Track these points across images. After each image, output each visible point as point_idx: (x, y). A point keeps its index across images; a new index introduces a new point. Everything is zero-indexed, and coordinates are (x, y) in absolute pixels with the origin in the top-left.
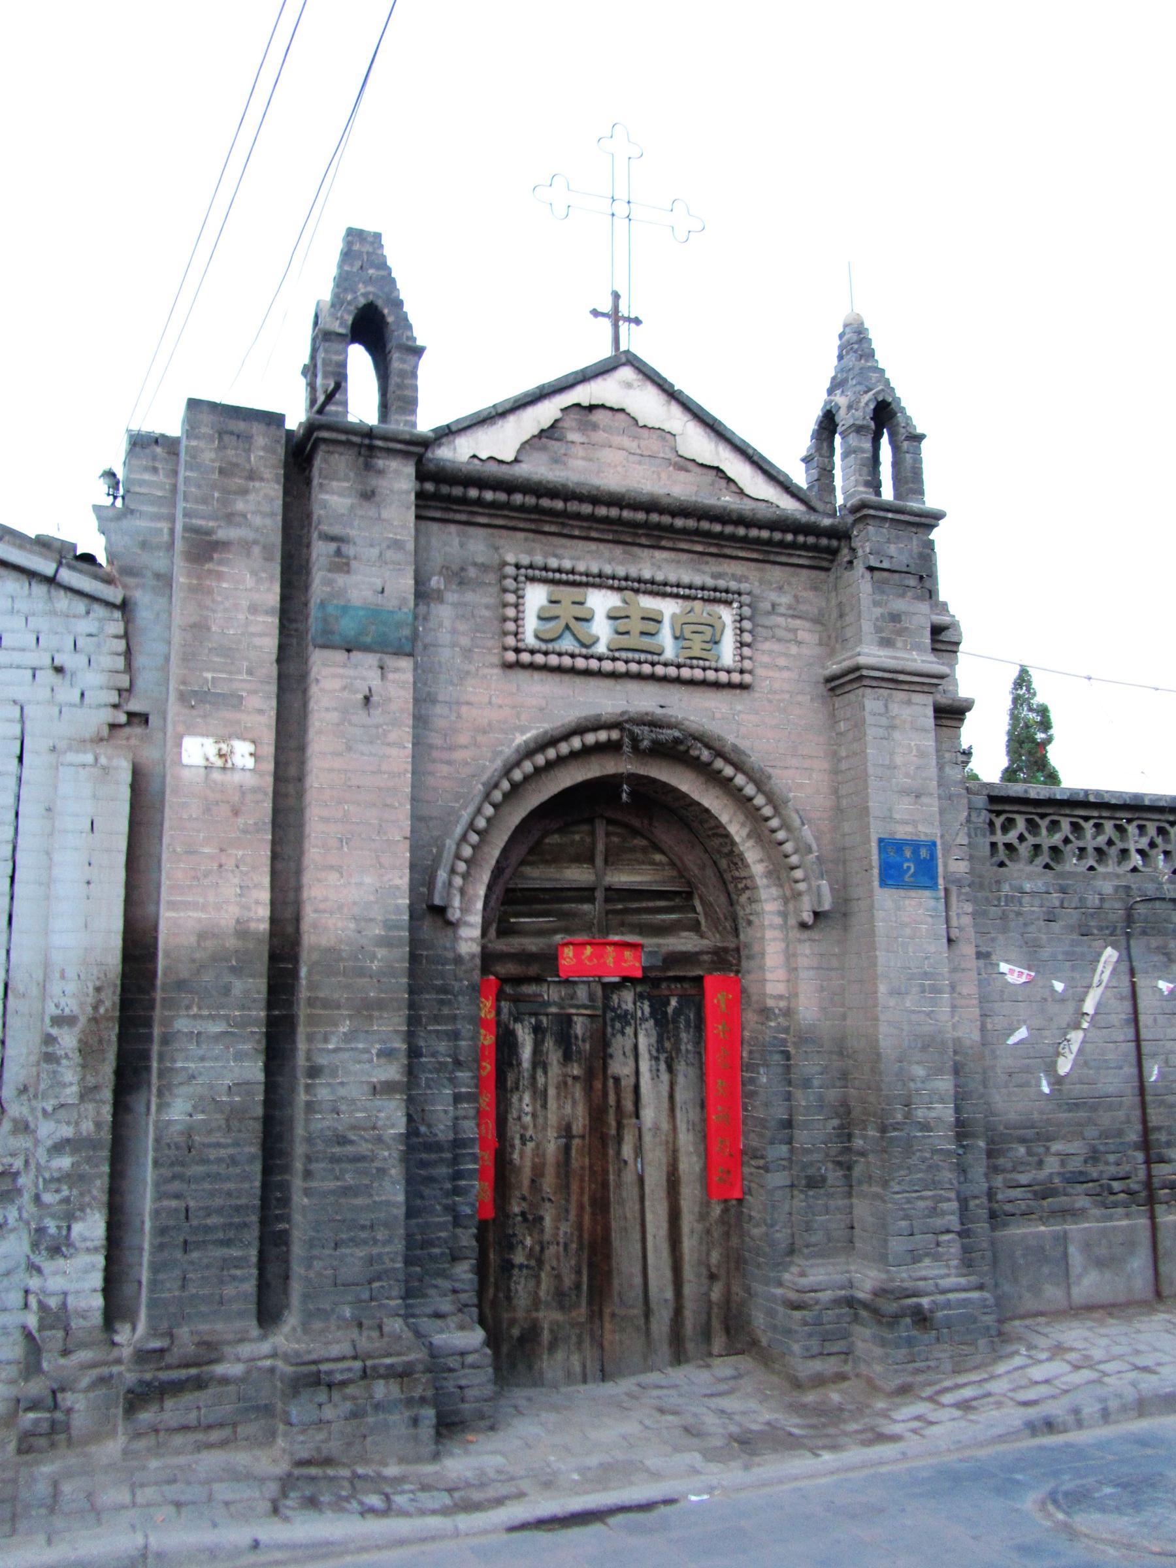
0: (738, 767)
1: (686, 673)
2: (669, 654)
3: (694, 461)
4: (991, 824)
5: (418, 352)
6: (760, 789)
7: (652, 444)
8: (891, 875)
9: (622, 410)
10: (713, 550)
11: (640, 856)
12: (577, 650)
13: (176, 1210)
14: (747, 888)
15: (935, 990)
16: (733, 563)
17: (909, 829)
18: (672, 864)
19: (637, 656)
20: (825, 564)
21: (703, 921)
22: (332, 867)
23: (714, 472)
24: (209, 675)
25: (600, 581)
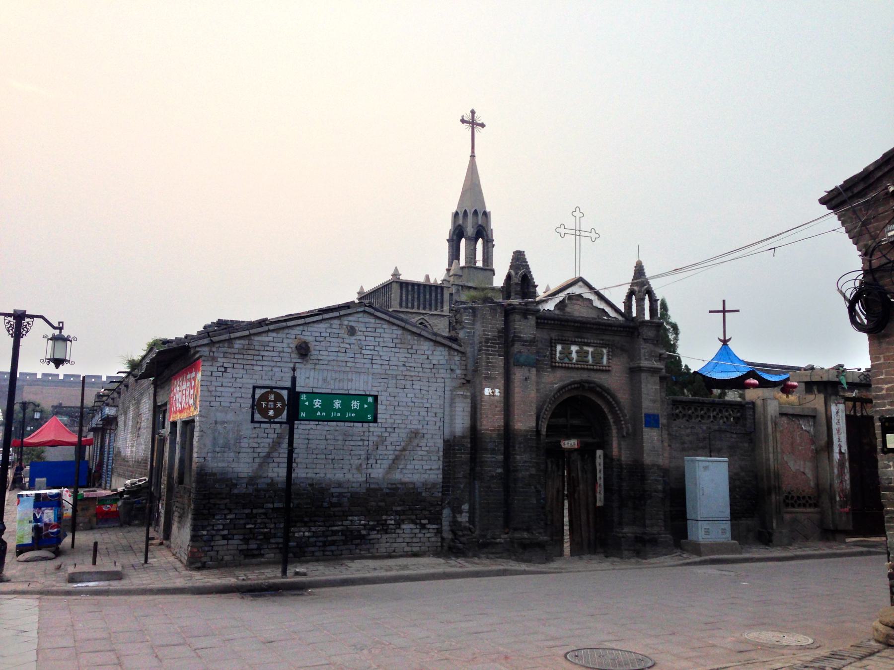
1: (595, 367)
4: (672, 408)
5: (536, 286)
8: (648, 425)
12: (568, 362)
15: (658, 455)
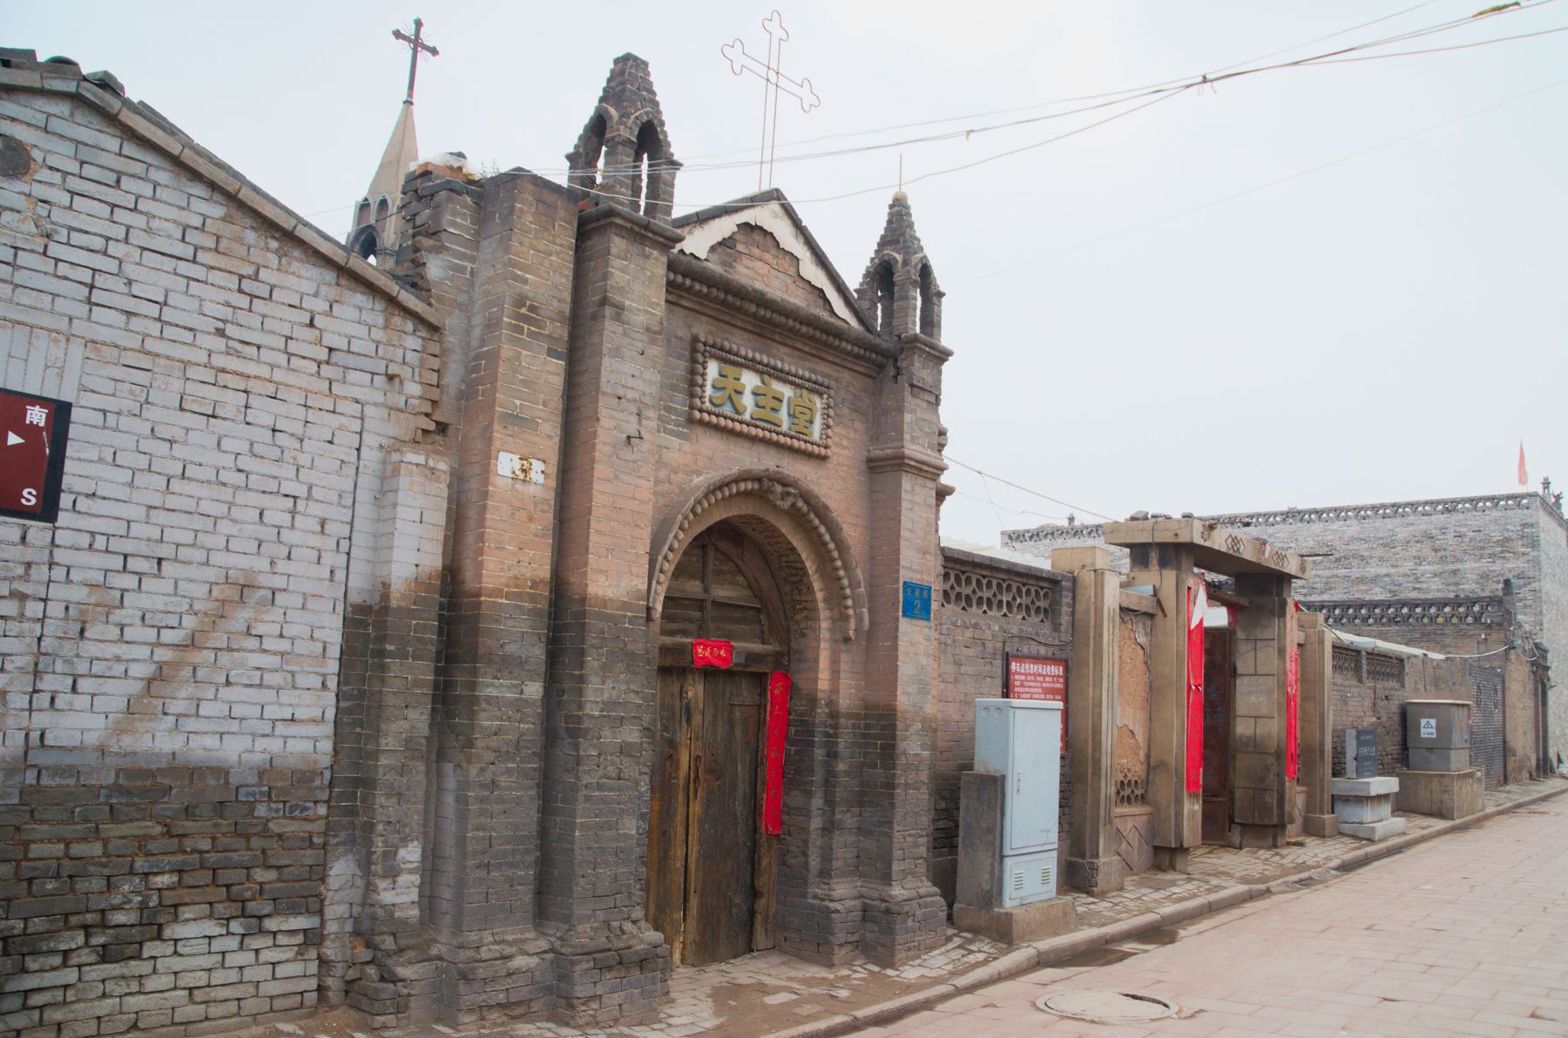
0: (823, 522)
2: (785, 428)
3: (809, 282)
6: (833, 539)
7: (786, 263)
9: (771, 234)
10: (838, 361)
11: (729, 577)
13: (484, 838)
14: (805, 609)
16: (823, 363)
17: (919, 576)
18: (750, 587)
19: (769, 426)
20: (874, 374)
21: (1347, 637)
22: (601, 572)
23: (817, 292)
24: (518, 402)
25: (752, 365)
